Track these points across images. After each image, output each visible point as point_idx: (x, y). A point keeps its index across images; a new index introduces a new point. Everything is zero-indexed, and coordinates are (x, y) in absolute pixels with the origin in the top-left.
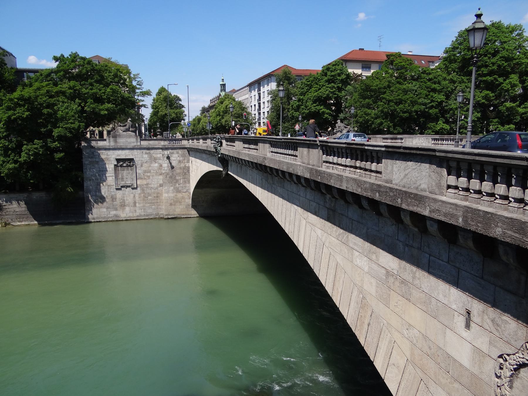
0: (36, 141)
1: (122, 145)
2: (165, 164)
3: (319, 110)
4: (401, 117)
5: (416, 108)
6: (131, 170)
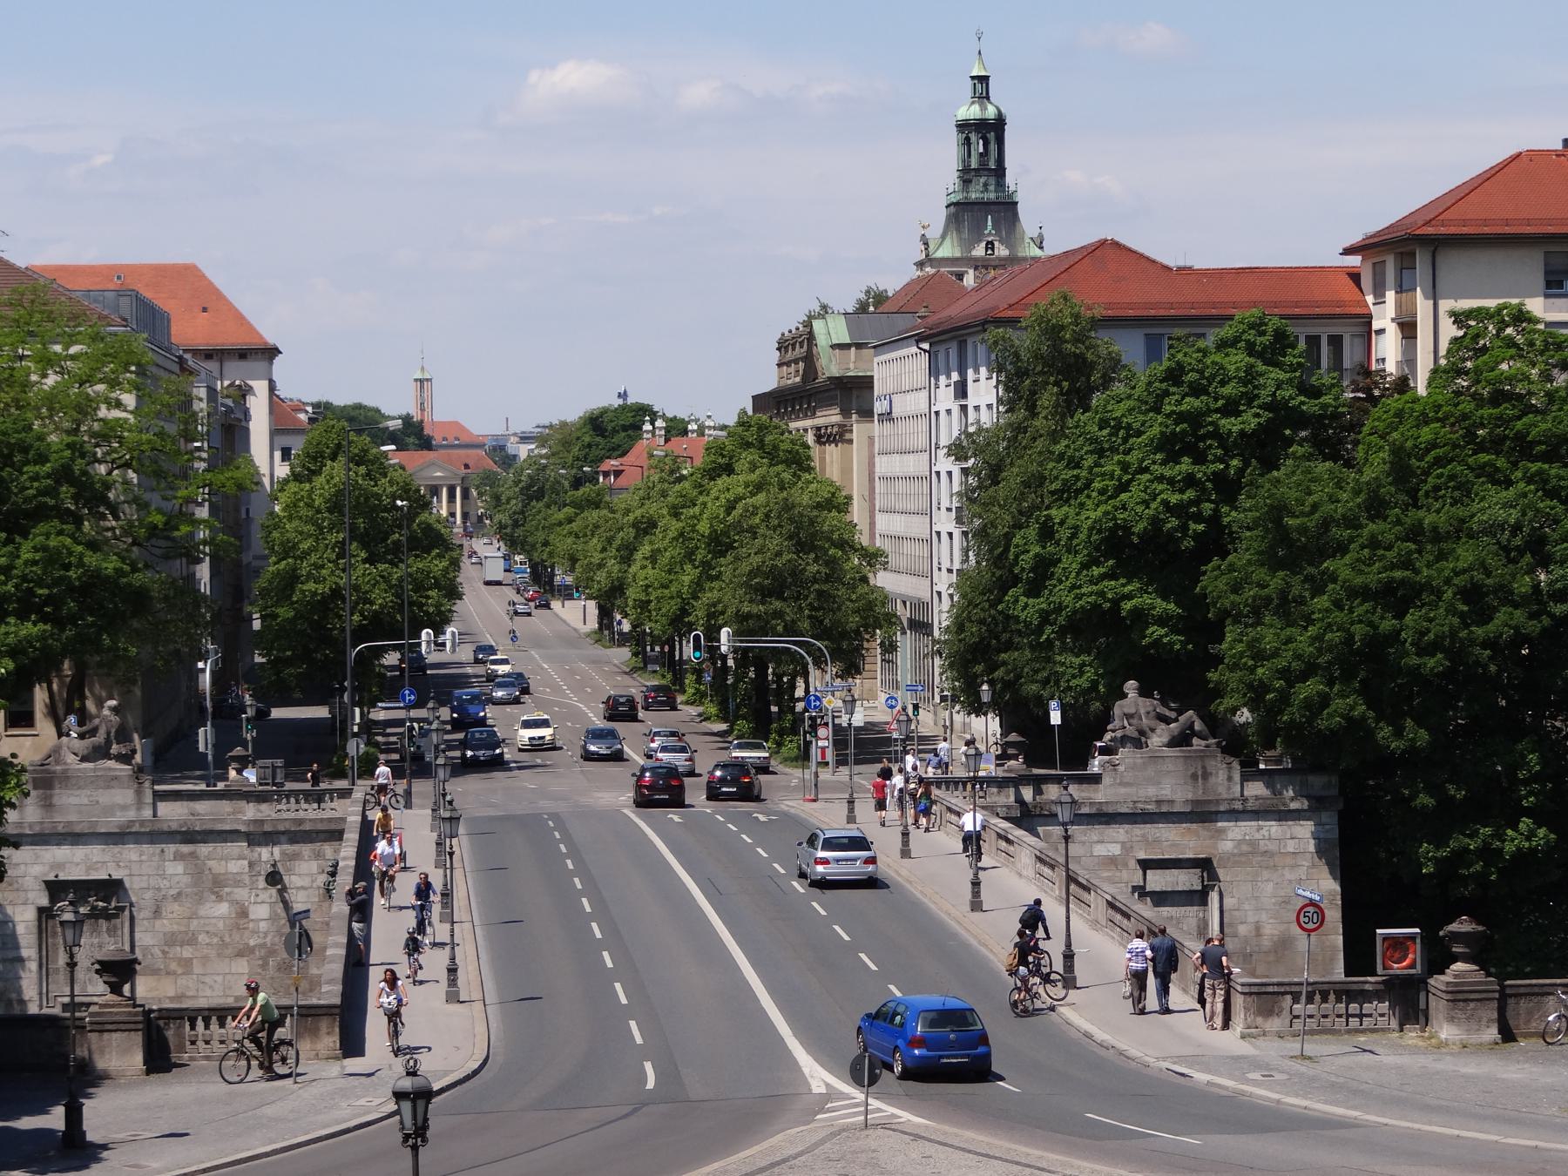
0: (815, 1090)
1: (73, 818)
2: (263, 907)
3: (1116, 603)
4: (1415, 672)
5: (1504, 621)
6: (112, 932)
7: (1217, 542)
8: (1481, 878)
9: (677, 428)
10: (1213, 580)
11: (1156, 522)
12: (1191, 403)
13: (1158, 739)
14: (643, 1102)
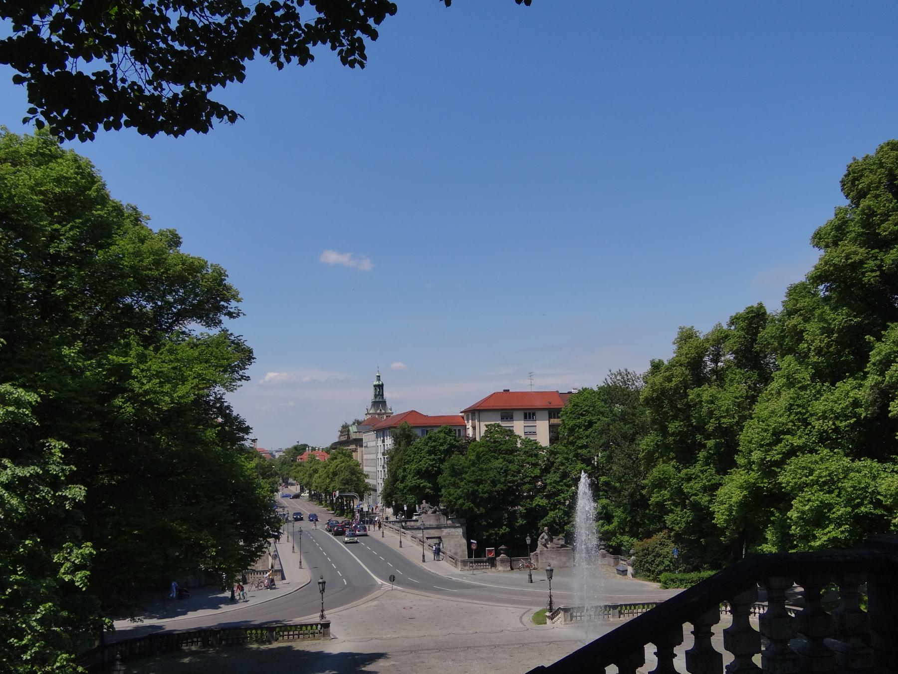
5: (499, 487)
7: (439, 472)
8: (495, 539)
9: (314, 449)
10: (440, 479)
11: (427, 468)
12: (434, 444)
13: (430, 512)
14: (346, 587)
